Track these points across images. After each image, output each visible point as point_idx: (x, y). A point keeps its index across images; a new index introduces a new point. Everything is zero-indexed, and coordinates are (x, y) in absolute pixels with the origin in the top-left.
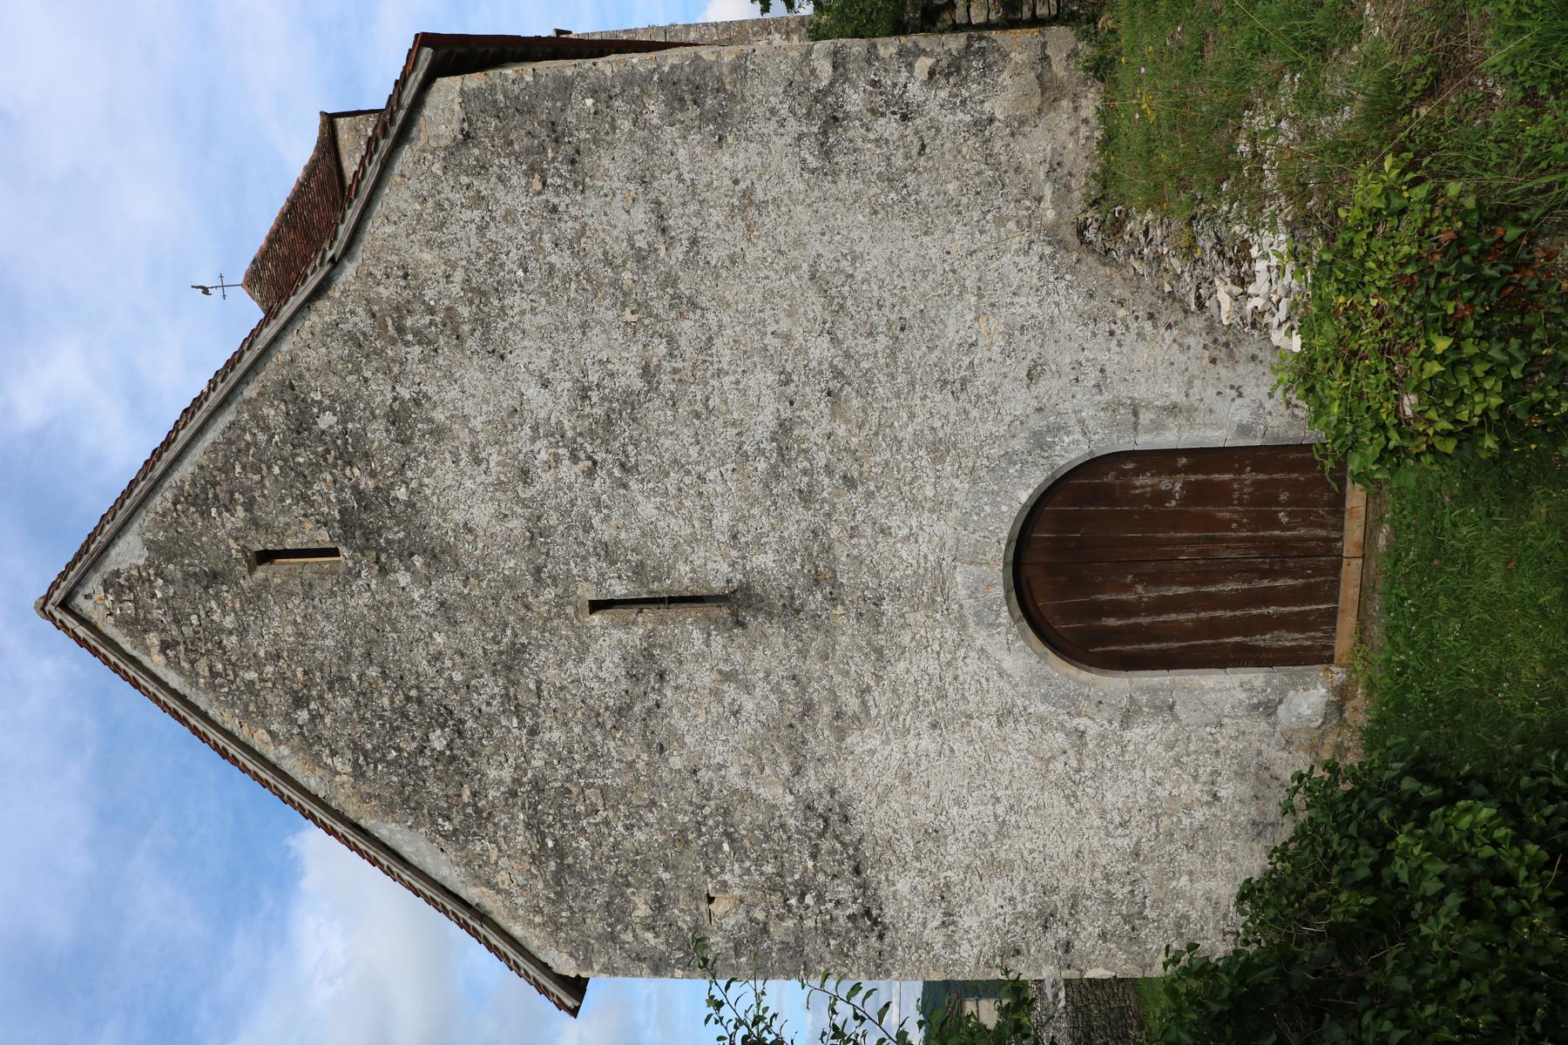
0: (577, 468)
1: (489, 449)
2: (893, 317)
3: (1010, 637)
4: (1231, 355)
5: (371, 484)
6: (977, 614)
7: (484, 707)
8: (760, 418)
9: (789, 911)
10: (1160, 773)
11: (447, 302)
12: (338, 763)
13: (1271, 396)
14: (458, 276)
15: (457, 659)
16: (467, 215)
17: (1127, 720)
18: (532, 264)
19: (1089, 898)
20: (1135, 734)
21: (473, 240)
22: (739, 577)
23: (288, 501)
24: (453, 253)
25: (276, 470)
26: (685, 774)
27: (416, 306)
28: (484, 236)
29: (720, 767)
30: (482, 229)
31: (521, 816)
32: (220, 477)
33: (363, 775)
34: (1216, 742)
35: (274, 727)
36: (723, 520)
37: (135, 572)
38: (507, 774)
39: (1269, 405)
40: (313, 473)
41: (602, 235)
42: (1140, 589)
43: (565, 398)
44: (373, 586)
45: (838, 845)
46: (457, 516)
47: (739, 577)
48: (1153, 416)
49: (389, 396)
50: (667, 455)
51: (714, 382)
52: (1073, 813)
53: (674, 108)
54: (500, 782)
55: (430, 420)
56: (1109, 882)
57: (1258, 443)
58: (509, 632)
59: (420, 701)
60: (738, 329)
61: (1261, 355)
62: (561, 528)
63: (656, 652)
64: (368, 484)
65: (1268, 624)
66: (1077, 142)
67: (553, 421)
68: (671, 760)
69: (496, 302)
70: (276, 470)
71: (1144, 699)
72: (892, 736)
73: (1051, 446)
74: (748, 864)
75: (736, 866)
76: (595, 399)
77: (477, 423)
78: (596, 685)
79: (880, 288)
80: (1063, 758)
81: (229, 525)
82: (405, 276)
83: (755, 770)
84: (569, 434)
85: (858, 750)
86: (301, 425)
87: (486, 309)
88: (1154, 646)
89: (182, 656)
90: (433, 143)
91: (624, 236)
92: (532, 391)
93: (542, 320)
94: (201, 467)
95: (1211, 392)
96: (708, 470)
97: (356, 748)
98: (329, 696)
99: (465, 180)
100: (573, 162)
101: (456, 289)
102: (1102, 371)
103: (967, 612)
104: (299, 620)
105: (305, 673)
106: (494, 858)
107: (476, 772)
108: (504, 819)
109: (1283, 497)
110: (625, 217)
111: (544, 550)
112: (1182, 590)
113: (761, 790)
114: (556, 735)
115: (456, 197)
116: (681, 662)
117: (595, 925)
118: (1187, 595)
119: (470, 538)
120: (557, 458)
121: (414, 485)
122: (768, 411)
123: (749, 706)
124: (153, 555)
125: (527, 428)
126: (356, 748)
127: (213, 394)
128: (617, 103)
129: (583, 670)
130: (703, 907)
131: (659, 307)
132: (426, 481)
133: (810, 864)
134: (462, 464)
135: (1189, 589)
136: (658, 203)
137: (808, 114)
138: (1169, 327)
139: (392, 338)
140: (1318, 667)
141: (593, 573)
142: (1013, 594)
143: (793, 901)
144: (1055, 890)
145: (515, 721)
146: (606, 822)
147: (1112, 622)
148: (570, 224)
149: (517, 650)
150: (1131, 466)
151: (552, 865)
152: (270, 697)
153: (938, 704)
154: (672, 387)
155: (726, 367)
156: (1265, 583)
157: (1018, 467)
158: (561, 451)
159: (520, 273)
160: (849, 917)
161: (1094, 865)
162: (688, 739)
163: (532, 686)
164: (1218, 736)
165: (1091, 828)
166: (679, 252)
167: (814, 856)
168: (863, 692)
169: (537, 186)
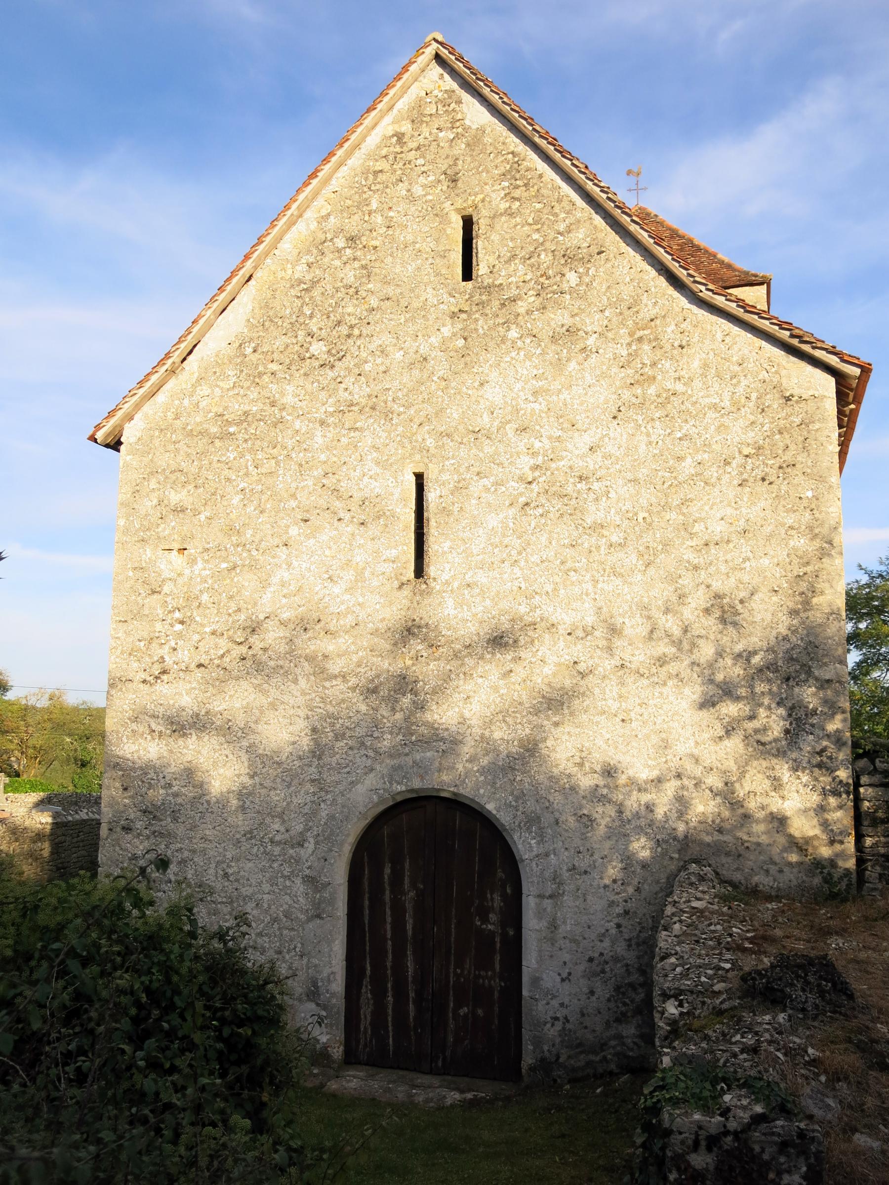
0: (527, 470)
1: (544, 403)
2: (633, 715)
3: (381, 792)
4: (595, 974)
5: (522, 311)
6: (400, 767)
7: (343, 386)
8: (559, 610)
9: (170, 612)
10: (266, 906)
11: (659, 377)
12: (301, 268)
13: (562, 1005)
14: (679, 387)
15: (383, 368)
16: (726, 397)
17: (311, 881)
18: (685, 443)
19: (167, 846)
20: (299, 887)
21: (707, 400)
22: (438, 587)
23: (511, 244)
24: (697, 384)
25: (536, 236)
26: (284, 538)
27: (659, 352)
28: (710, 408)
29: (289, 565)
30: (714, 407)
31: (255, 409)
32: (533, 192)
33: (292, 286)
34: (289, 951)
35: (332, 219)
36: (482, 578)
37: (459, 116)
38: (289, 400)
39: (555, 1003)
40: (532, 266)
41: (706, 498)
42: (412, 894)
43: (581, 464)
44: (442, 306)
45: (221, 652)
46: (494, 375)
47: (438, 587)
48: (549, 909)
49: (589, 329)
50: (534, 538)
51: (588, 577)
52: (238, 836)
53: (801, 558)
54: (282, 394)
55: (568, 360)
56: (179, 863)
57: (525, 993)
58: (402, 409)
59: (349, 336)
60: (629, 597)
61: (594, 998)
62: (481, 455)
63: (382, 521)
64: (521, 307)
65: (379, 994)
66: (765, 862)
67: (564, 454)
68: (296, 528)
69: (657, 415)
70: (536, 236)
71: (326, 895)
72: (308, 697)
73: (529, 830)
74: (210, 582)
75: (208, 572)
76: (579, 486)
77: (565, 395)
78: (358, 473)
79: (656, 706)
80: (283, 829)
81: (494, 195)
82: (682, 347)
83: (285, 591)
84: (553, 465)
85: (298, 671)
86: (569, 258)
87: (653, 407)
88: (367, 903)
89: (392, 149)
90: (783, 372)
91: (703, 515)
92: (587, 439)
93: (643, 448)
94: (541, 176)
95: (567, 957)
96: (521, 569)
97: (315, 283)
98: (357, 264)
99: (754, 396)
100: (763, 479)
101: (669, 385)
102: (586, 872)
103: (403, 759)
104: (417, 246)
105: (375, 248)
106: (221, 384)
107: (291, 375)
108: (253, 395)
109: (480, 1012)
110: (719, 516)
111: (465, 440)
112: (409, 927)
113: (269, 595)
114: (319, 439)
115: (740, 390)
116: (373, 539)
117: (164, 460)
118: (405, 931)
119: (476, 384)
120: (534, 454)
121: (519, 343)
122: (564, 616)
123: (337, 590)
124: (473, 132)
125: (560, 433)
126: (315, 283)
127: (598, 190)
128: (807, 514)
129: (370, 464)
130: (176, 546)
131: (648, 538)
132: (522, 353)
133: (208, 630)
134: (534, 382)
135: (410, 933)
136: (728, 541)
137: (792, 659)
138: (619, 926)
139: (634, 333)
140: (343, 1036)
141: (445, 477)
142: (414, 795)
143: (177, 615)
144: (175, 820)
145: (331, 409)
146: (247, 474)
147: (387, 871)
148: (715, 474)
149: (388, 415)
150: (509, 891)
151: (214, 430)
152: (356, 217)
153: (331, 734)
154: (586, 545)
155: (600, 586)
156: (412, 995)
157: (513, 803)
158: (540, 458)
159: (679, 435)
160: (162, 657)
161: (194, 851)
162: (312, 541)
163: (358, 425)
164: (293, 953)
165: (225, 850)
166: (690, 556)
167: (213, 633)
168: (344, 677)
169: (746, 451)
